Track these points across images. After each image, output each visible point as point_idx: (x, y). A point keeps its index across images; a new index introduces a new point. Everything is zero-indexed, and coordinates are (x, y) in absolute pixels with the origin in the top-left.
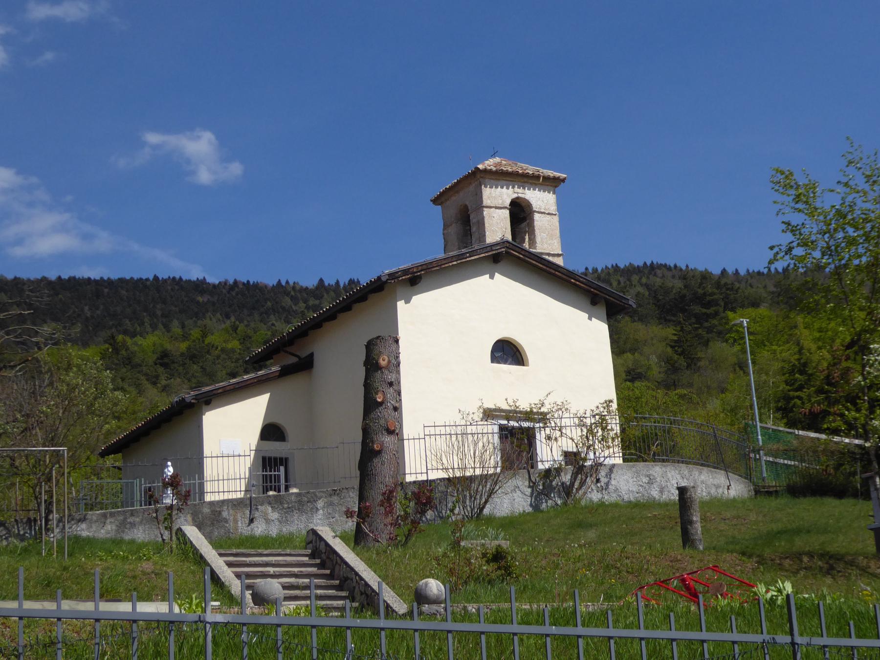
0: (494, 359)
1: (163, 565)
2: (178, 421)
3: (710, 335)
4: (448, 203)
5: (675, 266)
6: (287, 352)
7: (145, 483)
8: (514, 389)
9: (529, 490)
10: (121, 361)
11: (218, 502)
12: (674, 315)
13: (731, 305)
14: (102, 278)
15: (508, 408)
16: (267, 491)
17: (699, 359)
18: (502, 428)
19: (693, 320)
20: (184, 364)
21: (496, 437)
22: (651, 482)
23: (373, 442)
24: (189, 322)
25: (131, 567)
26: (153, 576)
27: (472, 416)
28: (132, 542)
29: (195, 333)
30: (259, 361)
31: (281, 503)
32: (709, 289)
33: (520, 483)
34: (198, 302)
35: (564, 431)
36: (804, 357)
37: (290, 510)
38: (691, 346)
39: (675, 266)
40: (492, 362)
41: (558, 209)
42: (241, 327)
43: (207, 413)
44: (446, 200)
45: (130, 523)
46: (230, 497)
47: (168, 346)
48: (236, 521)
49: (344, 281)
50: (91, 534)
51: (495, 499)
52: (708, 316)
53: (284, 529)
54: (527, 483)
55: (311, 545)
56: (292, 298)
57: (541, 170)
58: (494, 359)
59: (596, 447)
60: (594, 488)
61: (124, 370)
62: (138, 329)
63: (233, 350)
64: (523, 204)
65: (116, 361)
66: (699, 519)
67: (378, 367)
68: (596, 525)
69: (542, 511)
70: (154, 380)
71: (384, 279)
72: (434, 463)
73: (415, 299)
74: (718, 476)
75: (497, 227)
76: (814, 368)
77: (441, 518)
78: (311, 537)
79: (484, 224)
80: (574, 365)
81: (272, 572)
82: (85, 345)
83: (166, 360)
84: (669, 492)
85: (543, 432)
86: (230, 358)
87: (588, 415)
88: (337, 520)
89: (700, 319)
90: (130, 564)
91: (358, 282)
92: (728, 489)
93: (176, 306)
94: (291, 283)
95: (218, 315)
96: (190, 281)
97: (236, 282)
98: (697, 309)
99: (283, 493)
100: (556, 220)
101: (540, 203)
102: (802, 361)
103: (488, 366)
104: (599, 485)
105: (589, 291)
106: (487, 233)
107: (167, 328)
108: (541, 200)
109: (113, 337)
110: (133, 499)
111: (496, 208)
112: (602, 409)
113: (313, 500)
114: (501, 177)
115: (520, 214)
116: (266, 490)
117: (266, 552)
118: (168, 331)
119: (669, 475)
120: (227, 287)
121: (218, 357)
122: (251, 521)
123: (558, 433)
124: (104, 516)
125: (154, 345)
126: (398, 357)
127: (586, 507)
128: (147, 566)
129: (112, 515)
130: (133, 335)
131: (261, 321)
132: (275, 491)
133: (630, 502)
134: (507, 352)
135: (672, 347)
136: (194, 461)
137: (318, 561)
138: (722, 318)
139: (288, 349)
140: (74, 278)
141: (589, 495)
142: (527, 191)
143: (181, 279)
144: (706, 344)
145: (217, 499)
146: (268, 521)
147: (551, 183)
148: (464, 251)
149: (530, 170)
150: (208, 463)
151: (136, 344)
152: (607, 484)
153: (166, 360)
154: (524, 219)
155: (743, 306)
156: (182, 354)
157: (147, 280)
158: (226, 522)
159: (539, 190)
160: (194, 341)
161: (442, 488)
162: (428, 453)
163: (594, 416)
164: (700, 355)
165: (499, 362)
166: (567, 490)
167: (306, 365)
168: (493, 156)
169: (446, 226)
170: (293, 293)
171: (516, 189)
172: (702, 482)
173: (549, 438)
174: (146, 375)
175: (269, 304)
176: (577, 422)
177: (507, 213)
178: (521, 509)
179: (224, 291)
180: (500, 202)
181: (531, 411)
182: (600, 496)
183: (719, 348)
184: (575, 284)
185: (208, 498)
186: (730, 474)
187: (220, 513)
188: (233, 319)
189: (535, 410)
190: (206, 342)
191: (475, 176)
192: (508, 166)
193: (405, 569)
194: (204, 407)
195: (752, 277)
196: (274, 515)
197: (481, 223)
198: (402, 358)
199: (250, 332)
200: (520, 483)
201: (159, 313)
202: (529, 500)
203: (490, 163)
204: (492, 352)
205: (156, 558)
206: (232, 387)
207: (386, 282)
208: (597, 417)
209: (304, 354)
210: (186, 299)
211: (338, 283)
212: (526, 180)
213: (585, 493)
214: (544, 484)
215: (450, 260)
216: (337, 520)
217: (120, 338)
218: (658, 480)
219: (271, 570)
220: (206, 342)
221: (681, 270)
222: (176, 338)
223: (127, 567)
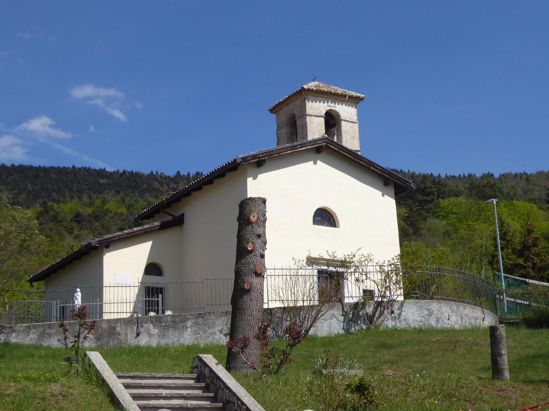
0: (315, 222)
1: (70, 387)
2: (85, 259)
3: (428, 214)
4: (281, 112)
5: (401, 171)
6: (165, 212)
7: (60, 304)
8: (328, 244)
9: (343, 318)
10: (48, 217)
11: (114, 320)
12: (405, 201)
13: (442, 195)
14: (40, 166)
15: (328, 257)
16: (149, 311)
17: (421, 229)
18: (320, 272)
19: (417, 204)
20: (90, 222)
21: (316, 279)
22: (430, 315)
23: (244, 282)
24: (94, 196)
25: (41, 389)
26: (61, 398)
27: (302, 262)
28: (49, 348)
29: (98, 202)
30: (138, 221)
31: (160, 322)
32: (429, 184)
33: (336, 313)
34: (100, 183)
35: (368, 276)
36: (505, 229)
37: (167, 327)
38: (416, 220)
39: (401, 171)
40: (314, 224)
41: (359, 119)
42: (127, 200)
43: (107, 254)
44: (280, 110)
45: (48, 334)
46: (122, 317)
47: (80, 210)
48: (126, 335)
49: (193, 173)
50: (18, 341)
51: (318, 324)
52: (427, 202)
53: (162, 342)
54: (341, 313)
55: (196, 370)
56: (160, 182)
57: (347, 91)
58: (315, 222)
59: (392, 288)
60: (389, 317)
61: (51, 224)
62: (62, 199)
63: (122, 214)
64: (334, 115)
65: (46, 218)
66: (506, 352)
67: (249, 222)
68: (395, 346)
69: (352, 334)
70: (70, 231)
71: (238, 161)
72: (274, 296)
73: (261, 177)
74: (477, 311)
75: (315, 129)
76: (512, 236)
77: (278, 336)
78: (197, 362)
79: (306, 127)
80: (370, 229)
81: (164, 395)
82: (28, 207)
83: (79, 219)
84: (443, 321)
85: (353, 276)
86: (120, 219)
87: (386, 264)
88: (201, 336)
89: (422, 203)
90: (41, 385)
91: (202, 174)
92: (483, 320)
93: (86, 185)
94: (159, 173)
95: (113, 192)
96: (95, 170)
97: (124, 171)
98: (420, 197)
99: (160, 315)
100: (356, 126)
101: (345, 114)
102: (503, 232)
103: (323, 224)
104: (393, 315)
105: (383, 176)
106: (309, 134)
107: (80, 198)
108: (347, 112)
109: (45, 203)
110: (51, 315)
111: (316, 116)
112: (396, 261)
113: (184, 320)
114: (320, 95)
115: (332, 121)
116: (147, 312)
117: (159, 375)
118: (81, 200)
119: (443, 309)
120: (119, 174)
121: (112, 218)
122: (138, 335)
123: (364, 277)
124: (29, 328)
125: (72, 209)
126: (265, 215)
127: (384, 332)
128: (55, 388)
129: (35, 327)
130: (58, 202)
131: (140, 196)
132: (155, 312)
133: (415, 328)
134: (324, 217)
135: (404, 220)
136: (95, 291)
137: (203, 385)
138: (436, 203)
139: (167, 210)
140: (22, 165)
141: (386, 323)
142: (337, 105)
143: (90, 168)
144: (425, 219)
145: (112, 318)
146: (150, 335)
147: (354, 101)
148: (291, 145)
149: (340, 91)
150: (106, 291)
151: (59, 208)
152: (400, 315)
153: (79, 219)
154: (334, 125)
155: (449, 196)
156: (89, 215)
157: (69, 168)
158: (119, 335)
159: (346, 105)
160: (97, 207)
161: (279, 315)
162: (269, 289)
163: (390, 265)
164: (421, 226)
165: (318, 224)
166: (370, 319)
167: (178, 222)
168: (314, 80)
169: (278, 128)
170: (160, 179)
171: (330, 104)
172: (466, 315)
173: (357, 280)
174: (66, 227)
175: (145, 186)
176: (379, 270)
177: (323, 120)
178: (336, 332)
179: (116, 176)
180: (318, 112)
181: (345, 260)
182: (393, 323)
183: (433, 222)
184: (373, 171)
185: (106, 317)
186: (484, 310)
187: (115, 328)
188: (122, 194)
189: (348, 260)
190: (105, 208)
191: (301, 94)
192: (324, 88)
193: (279, 395)
194: (105, 250)
195: (449, 179)
196: (155, 331)
197: (304, 127)
198: (267, 215)
199: (133, 202)
200: (336, 313)
201: (75, 189)
202: (342, 325)
203: (312, 85)
204: (314, 217)
205: (63, 380)
206: (125, 236)
207: (240, 164)
208: (393, 266)
209: (177, 214)
210: (93, 181)
211: (189, 174)
212: (336, 97)
213: (383, 321)
214: (353, 314)
215: (286, 150)
216: (201, 336)
217: (50, 204)
218: (435, 312)
219: (164, 392)
220: (105, 208)
221: (405, 173)
222: (86, 205)
223: (38, 389)
